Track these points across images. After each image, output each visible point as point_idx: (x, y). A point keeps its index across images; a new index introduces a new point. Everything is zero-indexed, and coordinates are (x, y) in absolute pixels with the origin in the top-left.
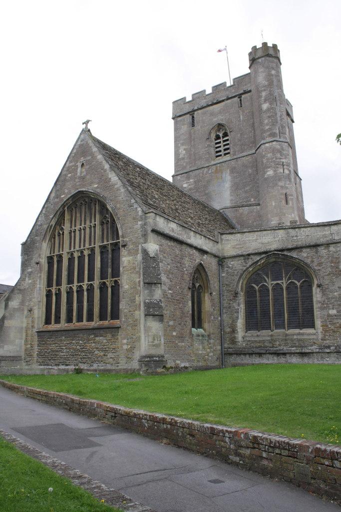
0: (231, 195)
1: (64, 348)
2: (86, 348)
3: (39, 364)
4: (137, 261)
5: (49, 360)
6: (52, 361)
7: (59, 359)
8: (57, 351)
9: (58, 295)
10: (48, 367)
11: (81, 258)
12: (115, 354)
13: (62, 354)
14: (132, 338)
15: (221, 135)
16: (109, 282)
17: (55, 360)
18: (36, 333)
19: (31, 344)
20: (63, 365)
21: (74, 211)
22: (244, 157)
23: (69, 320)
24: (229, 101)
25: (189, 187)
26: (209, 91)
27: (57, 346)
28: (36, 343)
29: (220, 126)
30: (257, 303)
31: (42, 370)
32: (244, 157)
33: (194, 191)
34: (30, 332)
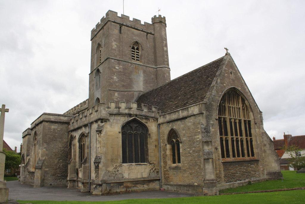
0: (144, 86)
1: (238, 171)
5: (231, 179)
6: (233, 179)
8: (235, 173)
9: (227, 141)
11: (235, 123)
13: (237, 175)
15: (136, 48)
16: (249, 138)
18: (222, 163)
19: (219, 170)
20: (238, 181)
21: (235, 98)
22: (150, 67)
23: (234, 156)
24: (142, 32)
25: (120, 70)
26: (119, 15)
28: (222, 169)
29: (137, 43)
31: (230, 185)
32: (150, 67)
33: (123, 74)
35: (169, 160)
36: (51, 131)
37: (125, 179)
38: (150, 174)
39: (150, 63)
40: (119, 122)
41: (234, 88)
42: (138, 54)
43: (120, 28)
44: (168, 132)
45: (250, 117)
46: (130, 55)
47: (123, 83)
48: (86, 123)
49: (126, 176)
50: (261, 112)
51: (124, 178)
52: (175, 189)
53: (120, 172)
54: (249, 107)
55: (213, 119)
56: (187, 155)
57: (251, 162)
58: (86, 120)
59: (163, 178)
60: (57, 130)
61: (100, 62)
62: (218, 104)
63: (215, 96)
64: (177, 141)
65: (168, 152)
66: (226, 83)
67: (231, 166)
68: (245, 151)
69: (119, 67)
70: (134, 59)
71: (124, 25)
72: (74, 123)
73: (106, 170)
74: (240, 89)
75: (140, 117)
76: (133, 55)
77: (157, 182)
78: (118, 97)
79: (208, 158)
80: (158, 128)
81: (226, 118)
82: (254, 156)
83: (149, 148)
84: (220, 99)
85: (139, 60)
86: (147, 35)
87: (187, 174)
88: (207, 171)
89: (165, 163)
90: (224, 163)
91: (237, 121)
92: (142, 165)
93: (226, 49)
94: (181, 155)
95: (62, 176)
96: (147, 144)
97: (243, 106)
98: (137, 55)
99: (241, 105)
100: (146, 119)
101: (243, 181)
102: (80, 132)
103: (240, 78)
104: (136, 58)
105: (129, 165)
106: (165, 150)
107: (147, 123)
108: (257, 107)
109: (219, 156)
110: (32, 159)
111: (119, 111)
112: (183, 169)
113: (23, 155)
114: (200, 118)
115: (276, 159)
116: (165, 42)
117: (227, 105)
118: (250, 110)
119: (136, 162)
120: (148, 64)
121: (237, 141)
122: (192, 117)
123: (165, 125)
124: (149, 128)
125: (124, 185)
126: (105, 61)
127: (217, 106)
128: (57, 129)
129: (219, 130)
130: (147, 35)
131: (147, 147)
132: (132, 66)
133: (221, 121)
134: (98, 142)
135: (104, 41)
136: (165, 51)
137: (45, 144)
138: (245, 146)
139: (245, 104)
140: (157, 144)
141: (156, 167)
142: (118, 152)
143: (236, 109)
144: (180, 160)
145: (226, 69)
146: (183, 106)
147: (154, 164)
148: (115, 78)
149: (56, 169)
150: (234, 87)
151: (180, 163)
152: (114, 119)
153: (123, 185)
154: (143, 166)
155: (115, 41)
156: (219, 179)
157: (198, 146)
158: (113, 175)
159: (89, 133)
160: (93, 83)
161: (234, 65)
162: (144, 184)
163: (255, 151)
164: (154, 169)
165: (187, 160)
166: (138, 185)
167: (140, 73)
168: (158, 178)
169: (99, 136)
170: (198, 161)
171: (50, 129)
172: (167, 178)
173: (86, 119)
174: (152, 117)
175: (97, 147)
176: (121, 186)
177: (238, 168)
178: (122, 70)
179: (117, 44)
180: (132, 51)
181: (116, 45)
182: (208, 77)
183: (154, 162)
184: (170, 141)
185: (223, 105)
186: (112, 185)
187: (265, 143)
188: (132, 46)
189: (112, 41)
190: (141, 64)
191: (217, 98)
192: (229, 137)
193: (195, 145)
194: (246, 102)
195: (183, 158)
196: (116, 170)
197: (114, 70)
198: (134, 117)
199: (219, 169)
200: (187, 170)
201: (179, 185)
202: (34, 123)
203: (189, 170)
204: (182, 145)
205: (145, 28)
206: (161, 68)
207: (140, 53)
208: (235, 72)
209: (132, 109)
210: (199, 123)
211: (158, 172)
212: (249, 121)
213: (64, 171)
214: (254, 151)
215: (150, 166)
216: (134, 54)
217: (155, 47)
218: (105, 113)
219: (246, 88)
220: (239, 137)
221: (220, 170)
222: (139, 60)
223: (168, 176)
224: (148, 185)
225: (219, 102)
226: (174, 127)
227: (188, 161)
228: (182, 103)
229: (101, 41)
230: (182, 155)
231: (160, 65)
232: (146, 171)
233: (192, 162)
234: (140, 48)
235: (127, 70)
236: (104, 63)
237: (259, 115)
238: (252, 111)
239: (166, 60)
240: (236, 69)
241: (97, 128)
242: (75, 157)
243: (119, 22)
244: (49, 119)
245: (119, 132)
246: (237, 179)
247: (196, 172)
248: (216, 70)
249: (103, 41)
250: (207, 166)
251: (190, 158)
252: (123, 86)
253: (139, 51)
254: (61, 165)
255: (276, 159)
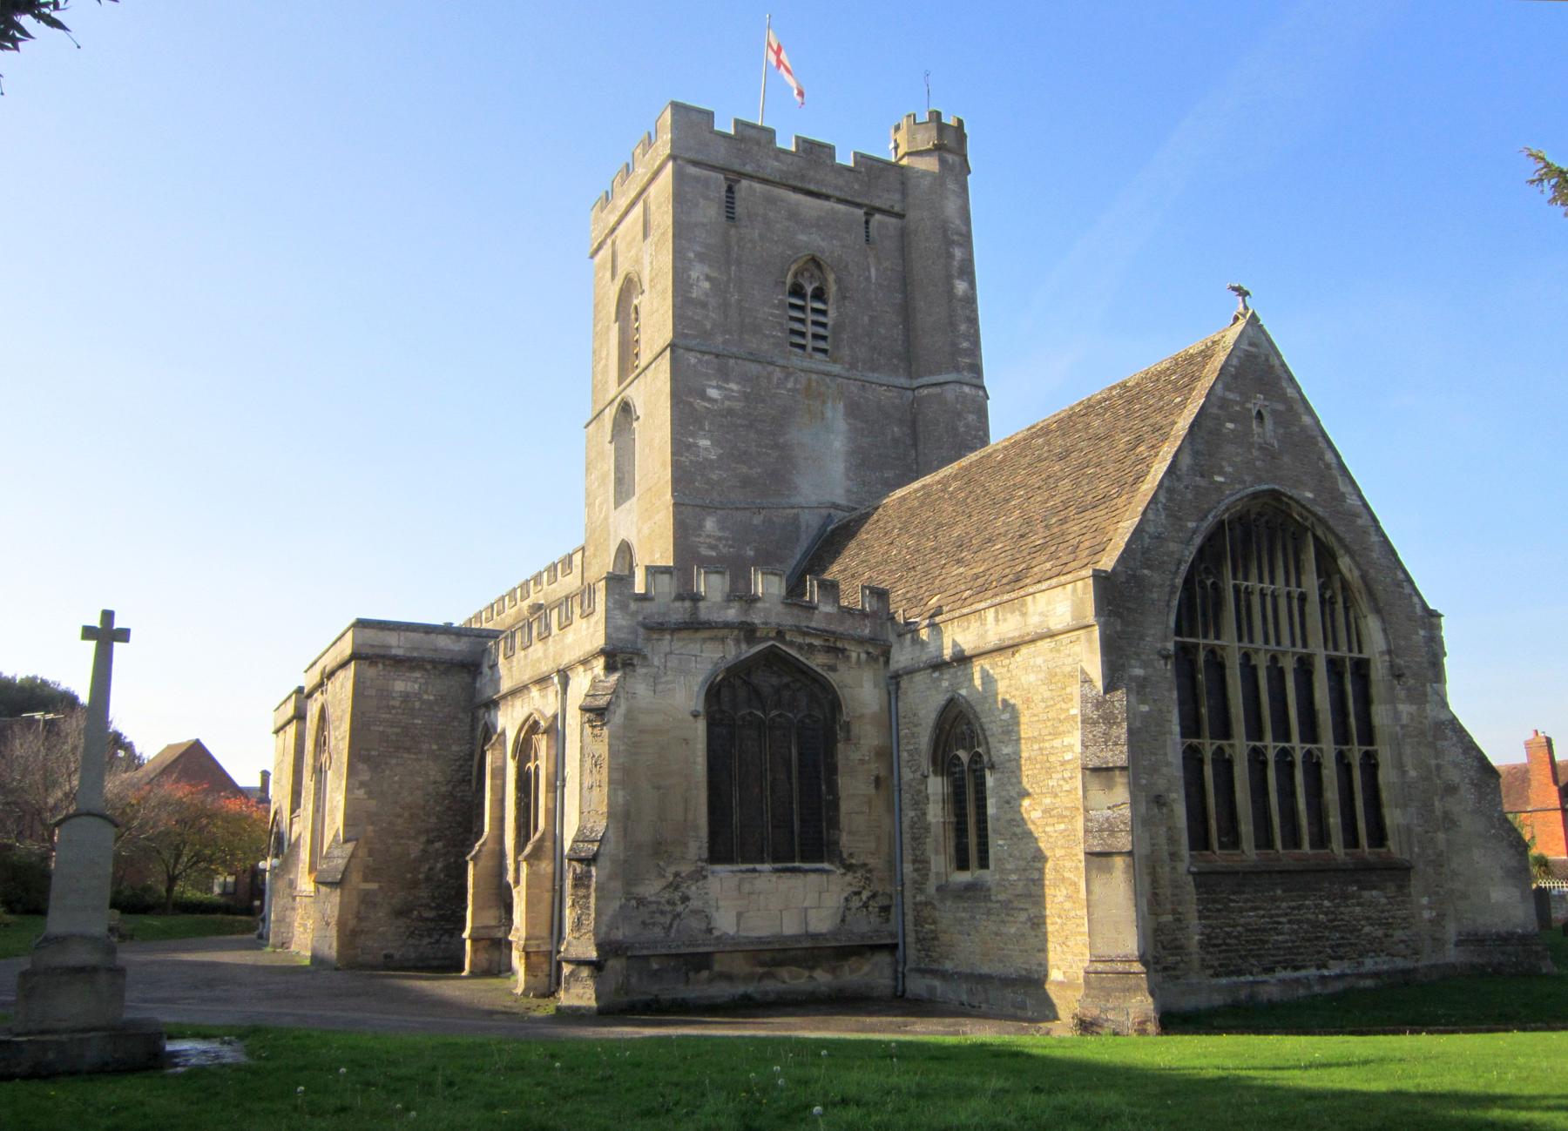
0: (848, 478)
1: (1283, 920)
2: (1342, 920)
3: (1211, 972)
4: (1426, 718)
6: (1253, 961)
7: (1272, 952)
8: (1264, 930)
9: (1224, 766)
10: (1242, 979)
11: (1277, 674)
12: (1408, 932)
14: (1437, 893)
15: (809, 290)
16: (1356, 752)
17: (1258, 956)
18: (1190, 878)
19: (1174, 912)
23: (1264, 839)
25: (727, 403)
27: (1263, 916)
28: (1191, 910)
34: (1165, 871)
35: (937, 852)
36: (394, 707)
37: (718, 938)
38: (849, 918)
39: (882, 362)
40: (693, 664)
41: (1275, 495)
42: (822, 319)
43: (730, 190)
45: (1365, 639)
46: (781, 324)
47: (744, 469)
49: (725, 923)
50: (1435, 615)
51: (716, 933)
52: (964, 998)
53: (695, 904)
54: (1363, 590)
55: (1144, 657)
57: (1364, 873)
58: (546, 657)
59: (910, 939)
60: (420, 699)
62: (1179, 581)
63: (1159, 537)
64: (976, 758)
65: (936, 813)
66: (1229, 469)
67: (1244, 892)
68: (1331, 820)
69: (726, 389)
70: (803, 347)
71: (750, 177)
73: (629, 896)
74: (1310, 495)
75: (800, 640)
76: (797, 326)
77: (883, 959)
78: (720, 539)
79: (1107, 849)
80: (889, 693)
81: (1223, 648)
82: (1326, 848)
83: (843, 793)
84: (1190, 553)
85: (824, 351)
86: (867, 222)
87: (1019, 925)
89: (921, 863)
90: (1204, 880)
91: (1289, 664)
92: (806, 871)
93: (1243, 293)
95: (442, 917)
96: (833, 770)
97: (1323, 588)
98: (815, 323)
99: (1311, 583)
100: (828, 652)
101: (1312, 972)
103: (1314, 437)
104: (809, 342)
105: (741, 871)
106: (920, 801)
107: (833, 668)
108: (1408, 590)
109: (1172, 840)
111: (695, 610)
112: (1002, 897)
113: (276, 813)
114: (1077, 648)
116: (958, 253)
117: (1229, 583)
118: (1364, 604)
119: (775, 860)
120: (874, 370)
122: (1044, 645)
124: (845, 695)
125: (717, 967)
126: (655, 359)
127: (1167, 589)
128: (418, 695)
129: (1181, 711)
130: (867, 222)
131: (833, 787)
132: (790, 385)
133: (1193, 664)
135: (651, 263)
136: (960, 300)
137: (361, 766)
138: (1332, 794)
139: (1339, 571)
140: (883, 773)
141: (877, 886)
142: (686, 810)
144: (987, 852)
145: (1231, 396)
147: (870, 871)
148: (704, 443)
149: (415, 884)
150: (1273, 491)
152: (671, 653)
153: (709, 967)
154: (812, 877)
155: (701, 258)
156: (1172, 955)
157: (1066, 787)
158: (661, 919)
161: (1279, 371)
162: (812, 968)
163: (1393, 817)
164: (865, 895)
166: (784, 973)
167: (829, 414)
168: (889, 941)
170: (1068, 864)
171: (384, 694)
172: (928, 942)
174: (861, 641)
175: (586, 785)
176: (698, 970)
177: (1284, 905)
178: (738, 406)
179: (714, 275)
180: (793, 306)
181: (708, 278)
182: (1139, 440)
184: (942, 760)
185: (1209, 582)
186: (655, 966)
187: (1454, 776)
188: (789, 280)
189: (690, 261)
190: (836, 369)
191: (1173, 546)
192: (1240, 746)
194: (1344, 563)
195: (1000, 842)
196: (677, 896)
197: (700, 404)
199: (1172, 903)
200: (1016, 904)
201: (981, 976)
202: (318, 664)
203: (1027, 906)
204: (996, 779)
205: (856, 187)
206: (937, 390)
207: (832, 313)
208: (1280, 407)
209: (759, 605)
211: (885, 909)
212: (1362, 669)
213: (453, 893)
214: (1388, 821)
215: (849, 877)
217: (905, 281)
218: (624, 623)
219: (1344, 488)
220: (1298, 747)
221: (1180, 910)
222: (824, 351)
223: (932, 931)
224: (833, 971)
225: (1184, 568)
228: (1007, 571)
231: (931, 373)
234: (832, 289)
235: (764, 401)
236: (649, 373)
237: (1422, 633)
238: (1378, 611)
239: (965, 345)
240: (1290, 391)
241: (587, 695)
243: (721, 163)
244: (379, 647)
245: (695, 715)
246: (1279, 962)
248: (1177, 405)
249: (646, 260)
252: (746, 482)
254: (439, 865)
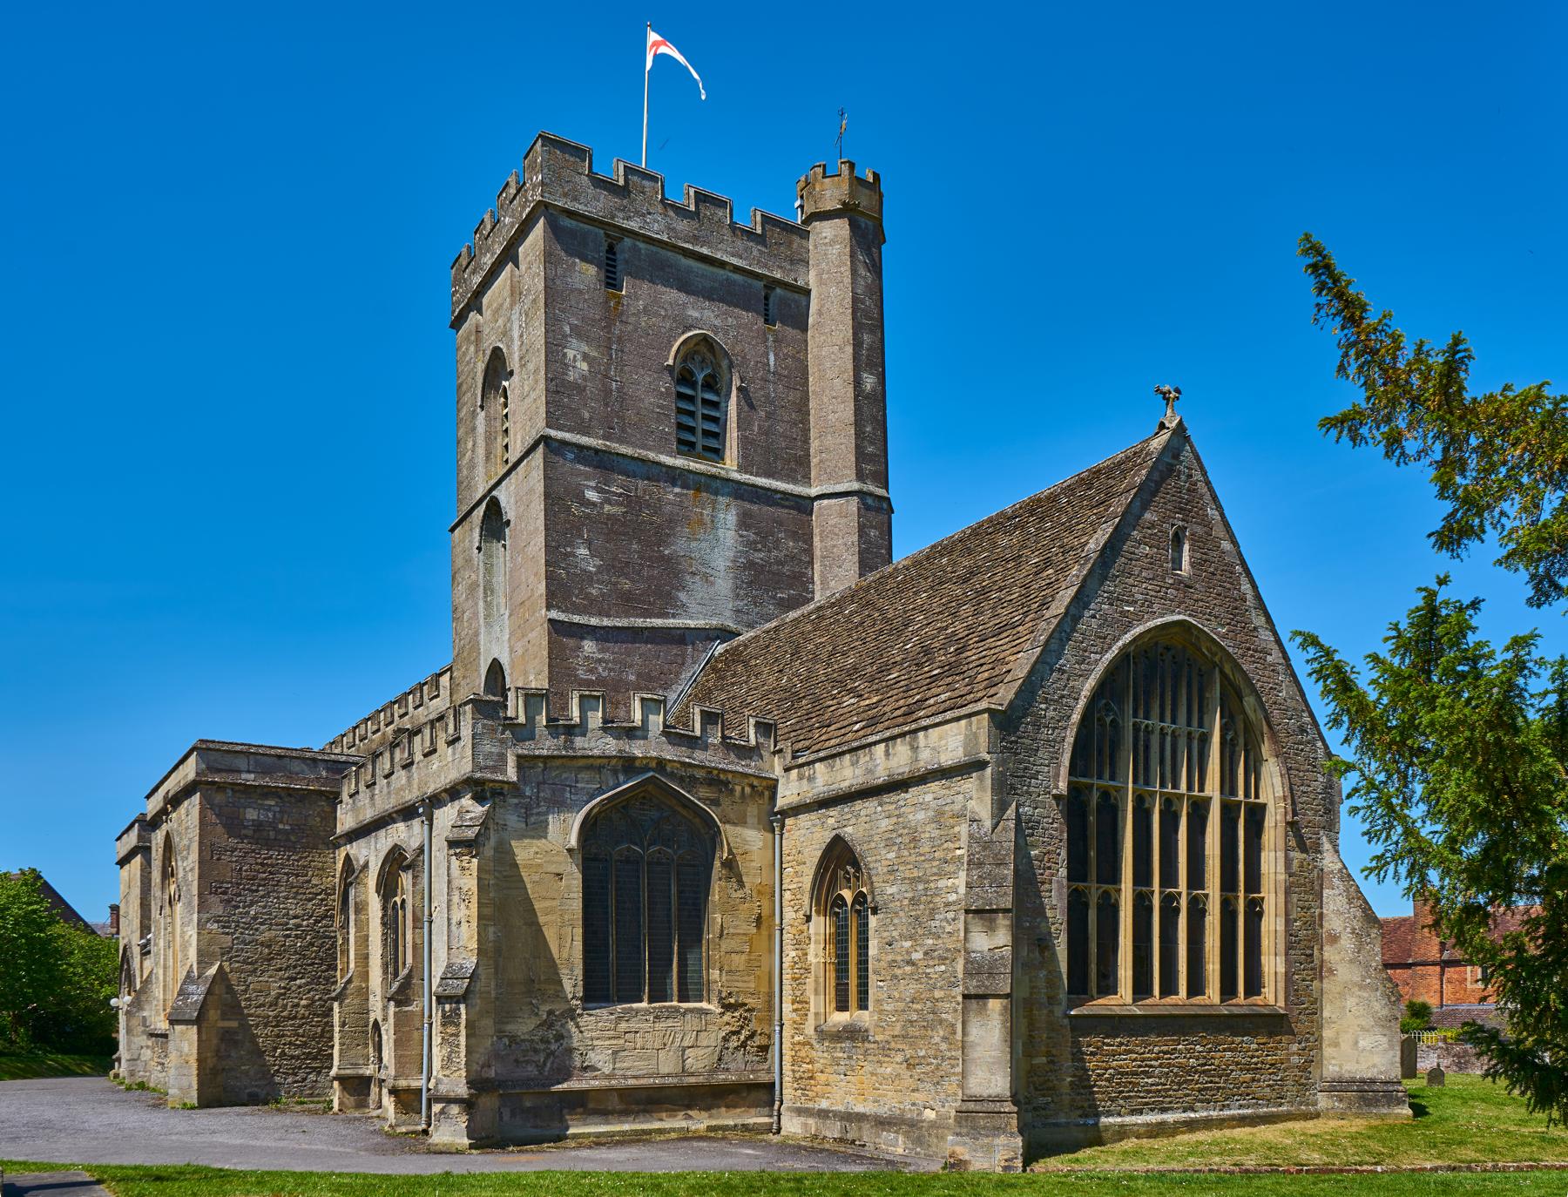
2: (1212, 1064)
3: (1079, 1112)
5: (1113, 1100)
6: (1121, 1102)
8: (1136, 1074)
15: (700, 377)
17: (1130, 1097)
19: (1048, 1054)
30: (608, 989)
38: (726, 1058)
40: (568, 795)
44: (819, 853)
48: (411, 796)
56: (898, 972)
60: (275, 829)
61: (507, 462)
64: (860, 898)
72: (361, 795)
73: (500, 1034)
78: (599, 661)
86: (766, 298)
88: (975, 1054)
94: (870, 970)
98: (706, 418)
102: (383, 841)
110: (161, 972)
115: (1385, 1012)
121: (1169, 914)
123: (804, 820)
134: (456, 899)
141: (753, 1025)
143: (1182, 742)
146: (901, 720)
148: (583, 551)
151: (866, 1008)
152: (544, 783)
156: (1044, 1096)
157: (949, 929)
159: (421, 850)
160: (474, 576)
165: (897, 996)
169: (463, 869)
173: (409, 778)
175: (454, 921)
180: (680, 396)
181: (585, 357)
182: (1048, 563)
183: (746, 1001)
185: (1108, 720)
189: (565, 336)
193: (937, 923)
194: (1249, 702)
196: (550, 1035)
198: (651, 774)
200: (893, 1045)
210: (960, 816)
211: (764, 1049)
216: (691, 414)
221: (1054, 1052)
226: (849, 830)
227: (901, 999)
228: (901, 703)
229: (506, 333)
230: (876, 972)
232: (705, 1043)
233: (918, 1007)
242: (367, 965)
246: (1147, 1104)
247: (935, 1058)
250: (975, 1032)
251: (912, 988)
253: (717, 393)
255: (1385, 1012)
